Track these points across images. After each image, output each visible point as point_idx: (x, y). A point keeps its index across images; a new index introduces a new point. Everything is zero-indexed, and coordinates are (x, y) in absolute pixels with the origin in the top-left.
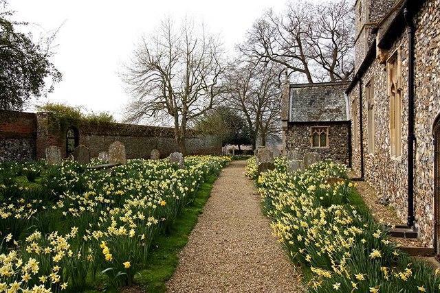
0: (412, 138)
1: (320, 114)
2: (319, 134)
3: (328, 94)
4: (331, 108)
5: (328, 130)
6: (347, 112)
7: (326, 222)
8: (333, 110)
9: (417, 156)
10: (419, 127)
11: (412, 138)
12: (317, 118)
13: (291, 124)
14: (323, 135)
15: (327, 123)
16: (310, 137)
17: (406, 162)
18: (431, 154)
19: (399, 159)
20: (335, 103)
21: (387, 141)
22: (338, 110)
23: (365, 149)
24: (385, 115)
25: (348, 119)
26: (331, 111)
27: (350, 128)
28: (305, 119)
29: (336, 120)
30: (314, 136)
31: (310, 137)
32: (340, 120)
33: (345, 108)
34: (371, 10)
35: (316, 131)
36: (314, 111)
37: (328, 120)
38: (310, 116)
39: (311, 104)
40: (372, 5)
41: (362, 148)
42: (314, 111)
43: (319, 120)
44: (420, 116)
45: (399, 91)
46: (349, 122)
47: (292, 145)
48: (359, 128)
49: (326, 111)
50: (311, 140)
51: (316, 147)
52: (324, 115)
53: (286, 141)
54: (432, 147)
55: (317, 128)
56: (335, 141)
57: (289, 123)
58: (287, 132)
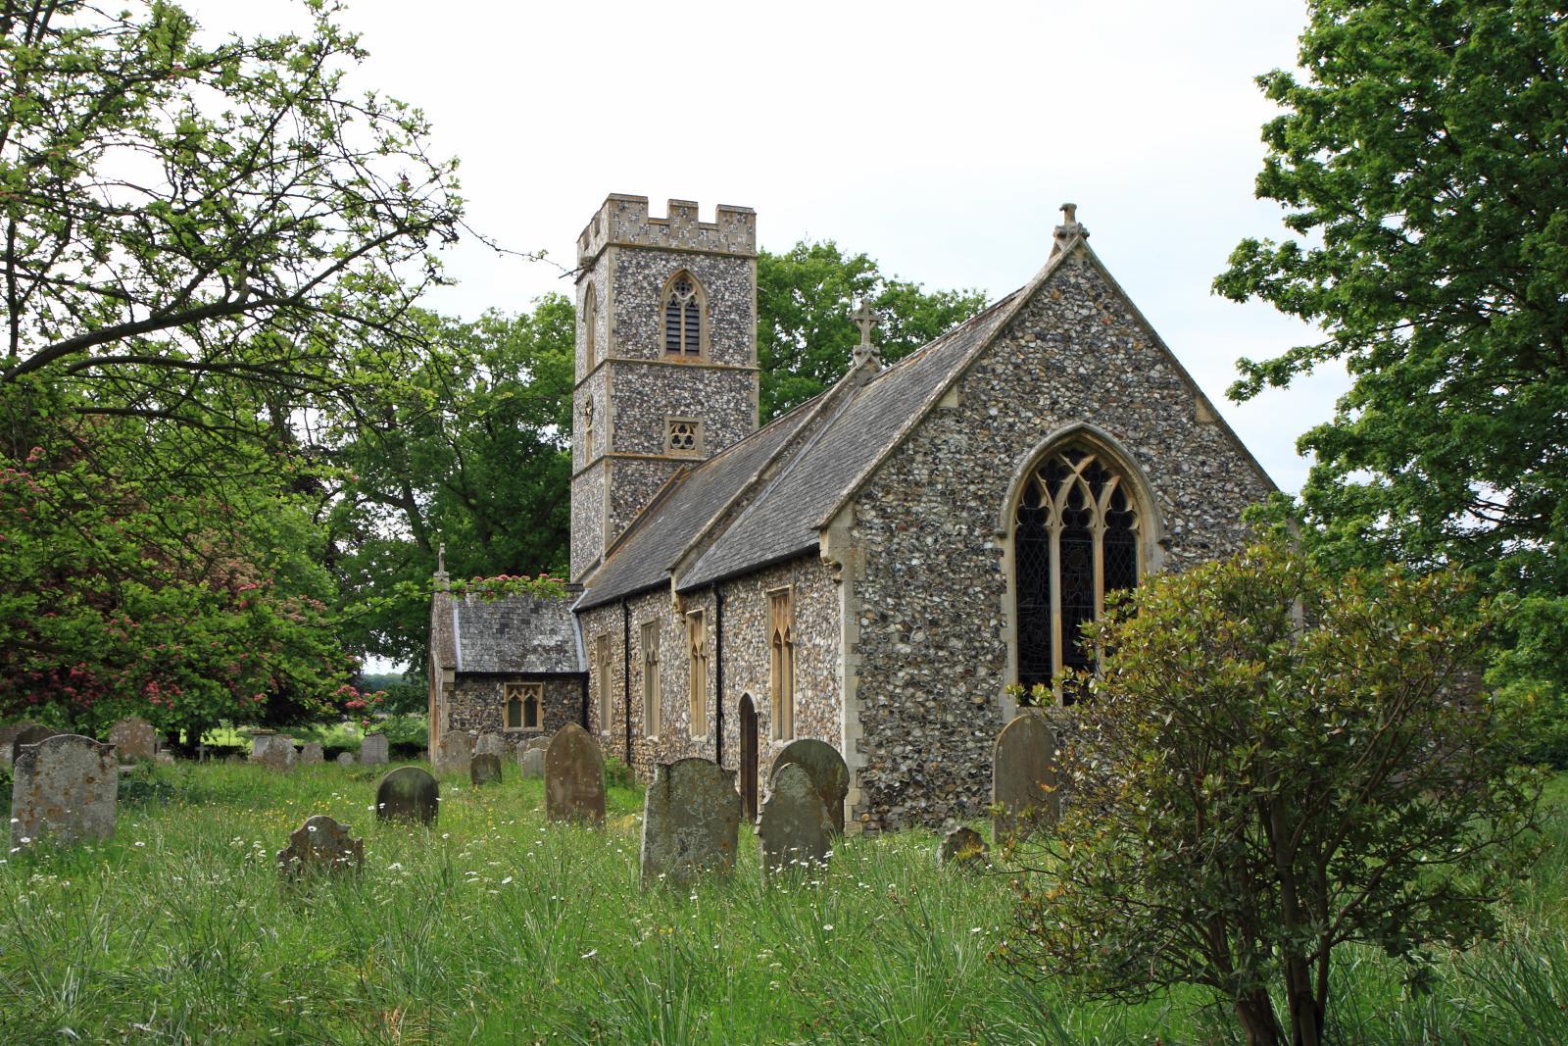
0: (720, 715)
1: (524, 656)
2: (523, 698)
3: (536, 610)
4: (545, 642)
5: (541, 691)
6: (580, 654)
7: (349, 995)
8: (551, 648)
9: (725, 734)
10: (727, 704)
11: (720, 715)
12: (519, 665)
13: (462, 677)
14: (531, 704)
15: (540, 677)
16: (503, 705)
17: (713, 741)
18: (738, 730)
19: (704, 739)
20: (553, 632)
21: (684, 716)
22: (560, 649)
23: (635, 731)
24: (682, 681)
25: (582, 669)
26: (547, 650)
27: (585, 687)
28: (492, 665)
29: (558, 670)
30: (514, 703)
31: (503, 705)
32: (567, 669)
33: (574, 645)
34: (617, 427)
35: (515, 692)
36: (508, 647)
37: (542, 670)
38: (502, 660)
39: (501, 631)
40: (619, 417)
41: (629, 729)
42: (508, 647)
43: (523, 670)
44: (728, 692)
45: (703, 658)
46: (584, 678)
47: (463, 724)
48: (714, 713)
49: (535, 650)
50: (505, 713)
51: (515, 729)
52: (532, 658)
53: (450, 715)
54: (739, 724)
55: (518, 688)
56: (555, 715)
57: (458, 675)
58: (452, 695)
